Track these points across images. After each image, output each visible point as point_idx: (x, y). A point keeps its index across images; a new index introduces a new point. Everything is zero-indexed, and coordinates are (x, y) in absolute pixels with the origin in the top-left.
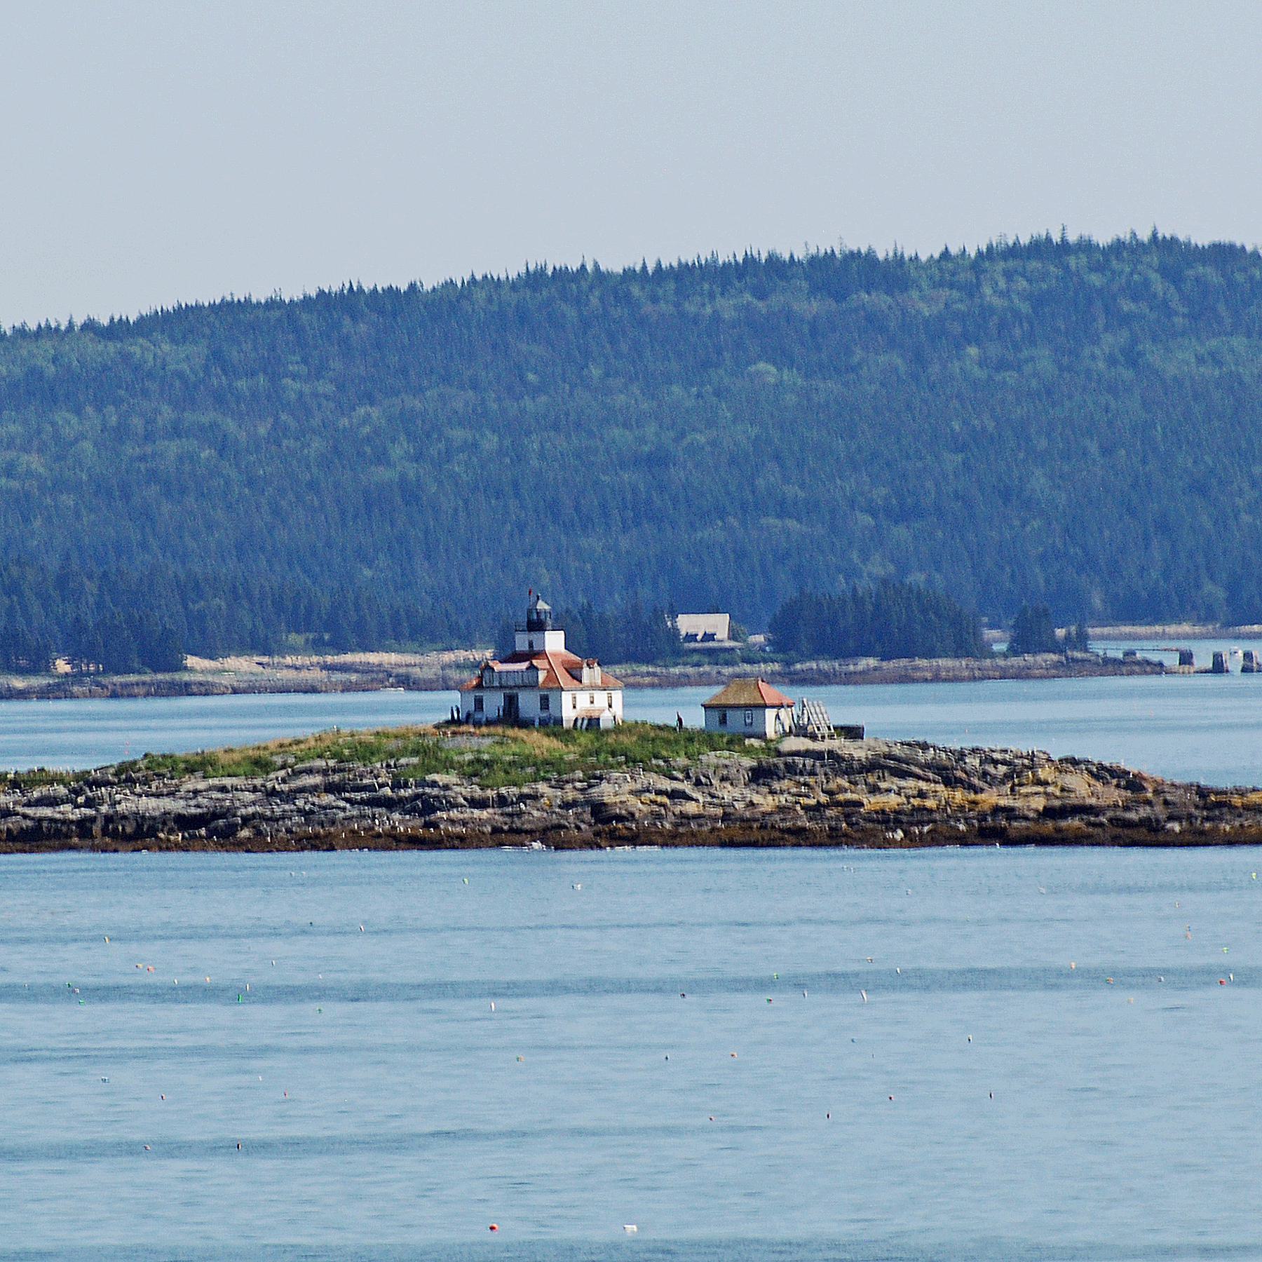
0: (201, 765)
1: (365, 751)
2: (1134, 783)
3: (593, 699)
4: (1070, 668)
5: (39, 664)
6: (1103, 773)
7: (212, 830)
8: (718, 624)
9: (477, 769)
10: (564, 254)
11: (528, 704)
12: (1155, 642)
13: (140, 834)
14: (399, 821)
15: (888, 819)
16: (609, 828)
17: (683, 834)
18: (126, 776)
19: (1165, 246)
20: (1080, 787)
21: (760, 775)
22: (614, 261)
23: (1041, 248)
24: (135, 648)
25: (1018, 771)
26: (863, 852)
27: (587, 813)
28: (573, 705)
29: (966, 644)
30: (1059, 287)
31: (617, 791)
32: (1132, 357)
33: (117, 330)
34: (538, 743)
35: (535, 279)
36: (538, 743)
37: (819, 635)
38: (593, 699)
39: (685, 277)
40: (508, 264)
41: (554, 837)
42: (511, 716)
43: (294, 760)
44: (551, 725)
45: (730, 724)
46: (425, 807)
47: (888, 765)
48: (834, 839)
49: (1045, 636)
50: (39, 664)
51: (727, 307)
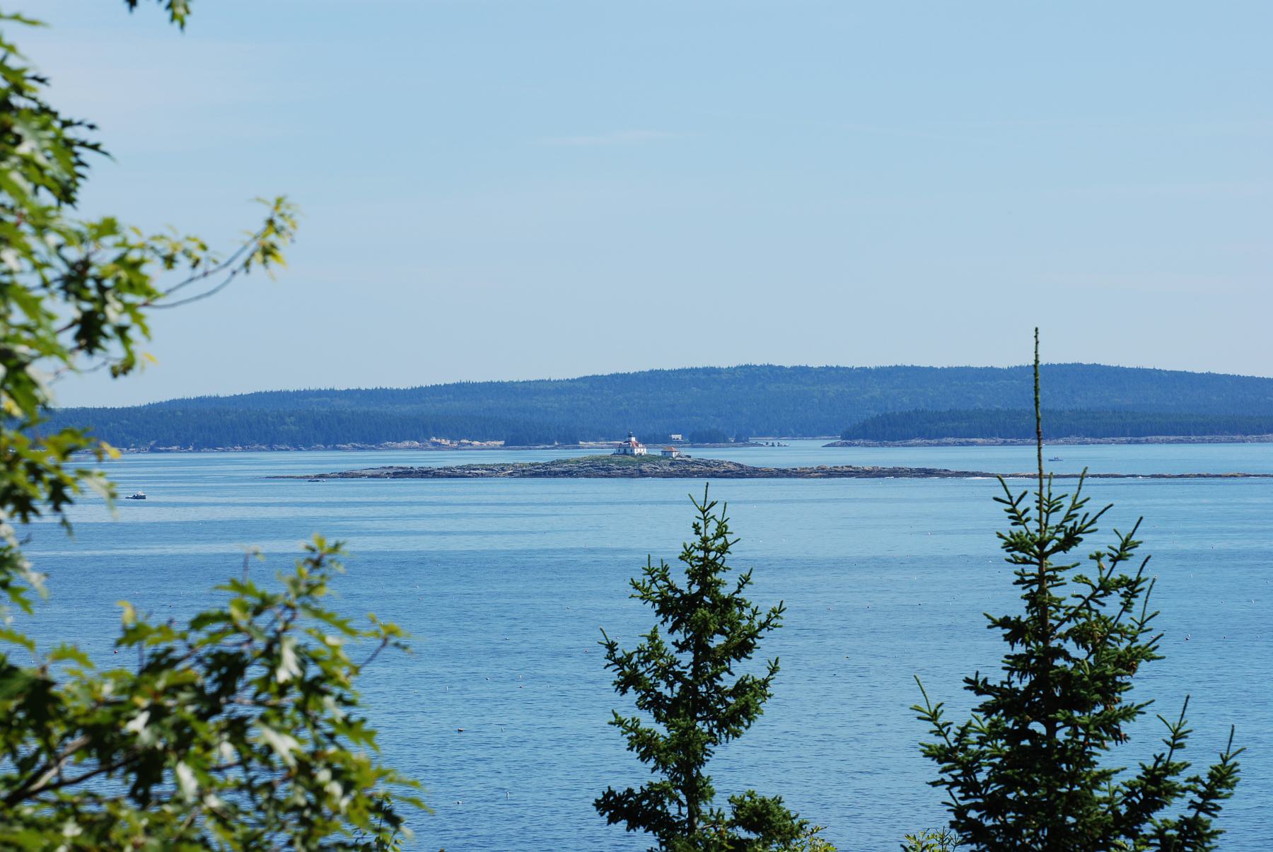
0: (567, 461)
1: (598, 460)
2: (741, 466)
3: (641, 450)
4: (745, 445)
5: (552, 443)
6: (736, 464)
7: (568, 474)
8: (679, 437)
9: (618, 463)
10: (178, 396)
11: (628, 451)
12: (762, 441)
13: (556, 475)
14: (603, 473)
15: (694, 473)
16: (643, 474)
17: (656, 475)
18: (553, 464)
19: (770, 366)
20: (731, 467)
21: (672, 464)
22: (223, 393)
23: (747, 366)
24: (570, 439)
25: (720, 464)
26: (140, 456)
27: (636, 471)
28: (636, 451)
29: (726, 441)
30: (750, 374)
31: (645, 467)
32: (763, 387)
33: (573, 380)
34: (630, 458)
35: (651, 372)
36: (630, 458)
37: (698, 439)
38: (641, 450)
39: (679, 371)
40: (646, 368)
41: (631, 476)
42: (625, 453)
43: (585, 461)
44: (633, 455)
45: (666, 455)
46: (608, 470)
47: (695, 463)
48: (684, 476)
49: (742, 439)
50: (552, 443)
51: (687, 377)
